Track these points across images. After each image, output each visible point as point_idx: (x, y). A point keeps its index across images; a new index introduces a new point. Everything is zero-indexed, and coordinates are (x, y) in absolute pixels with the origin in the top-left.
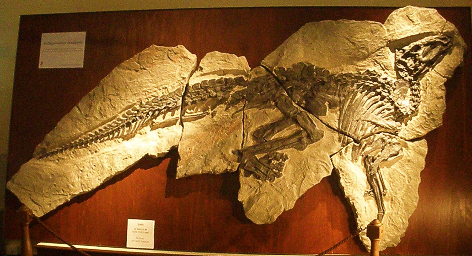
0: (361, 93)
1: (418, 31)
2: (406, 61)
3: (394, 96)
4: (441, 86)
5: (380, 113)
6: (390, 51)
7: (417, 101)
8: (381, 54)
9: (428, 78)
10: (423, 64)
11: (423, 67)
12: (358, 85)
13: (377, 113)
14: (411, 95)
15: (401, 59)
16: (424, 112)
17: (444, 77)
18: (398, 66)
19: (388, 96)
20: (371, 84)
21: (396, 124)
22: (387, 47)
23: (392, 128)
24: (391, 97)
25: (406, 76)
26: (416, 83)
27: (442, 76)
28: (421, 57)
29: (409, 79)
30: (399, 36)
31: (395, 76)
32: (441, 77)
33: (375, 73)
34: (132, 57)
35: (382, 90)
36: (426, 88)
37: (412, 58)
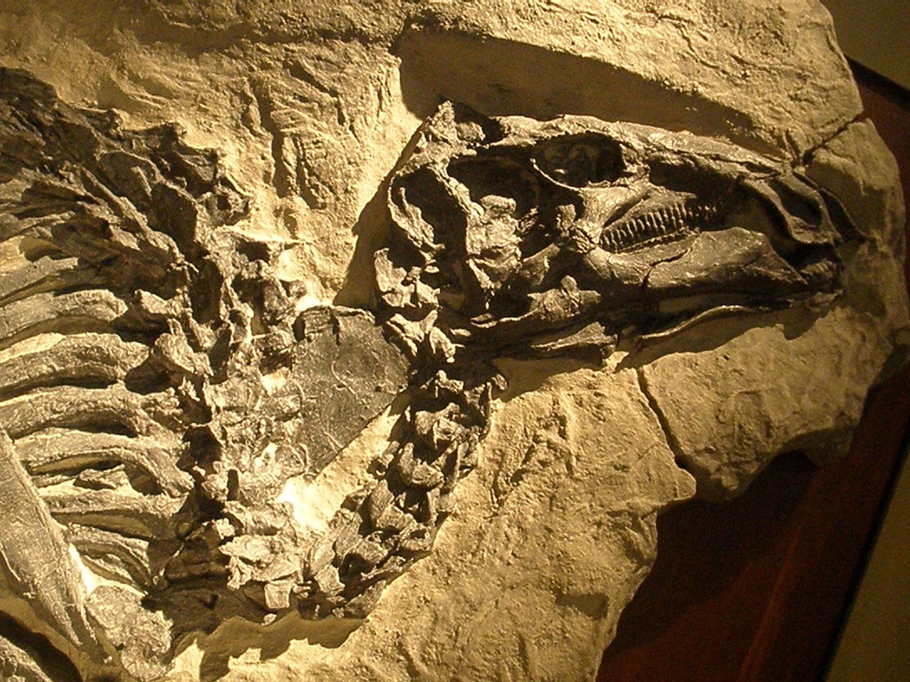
0: (33, 256)
1: (653, 58)
2: (475, 211)
3: (242, 399)
4: (634, 515)
5: (73, 473)
6: (396, 87)
7: (390, 532)
8: (322, 76)
9: (568, 407)
10: (582, 286)
11: (568, 304)
12: (38, 191)
13: (38, 457)
14: (375, 466)
15: (440, 169)
16: (400, 648)
17: (682, 461)
18: (393, 208)
19: (198, 382)
20: (131, 227)
21: (129, 625)
22: (393, 51)
23: (83, 634)
24: (215, 396)
25: (415, 312)
26: (458, 398)
27: (672, 441)
28: (593, 228)
29: (424, 345)
30: (512, 19)
31: (339, 272)
32: (669, 457)
33: (206, 174)
34: (383, 333)
35: (184, 319)
36: (518, 477)
37: (520, 213)
